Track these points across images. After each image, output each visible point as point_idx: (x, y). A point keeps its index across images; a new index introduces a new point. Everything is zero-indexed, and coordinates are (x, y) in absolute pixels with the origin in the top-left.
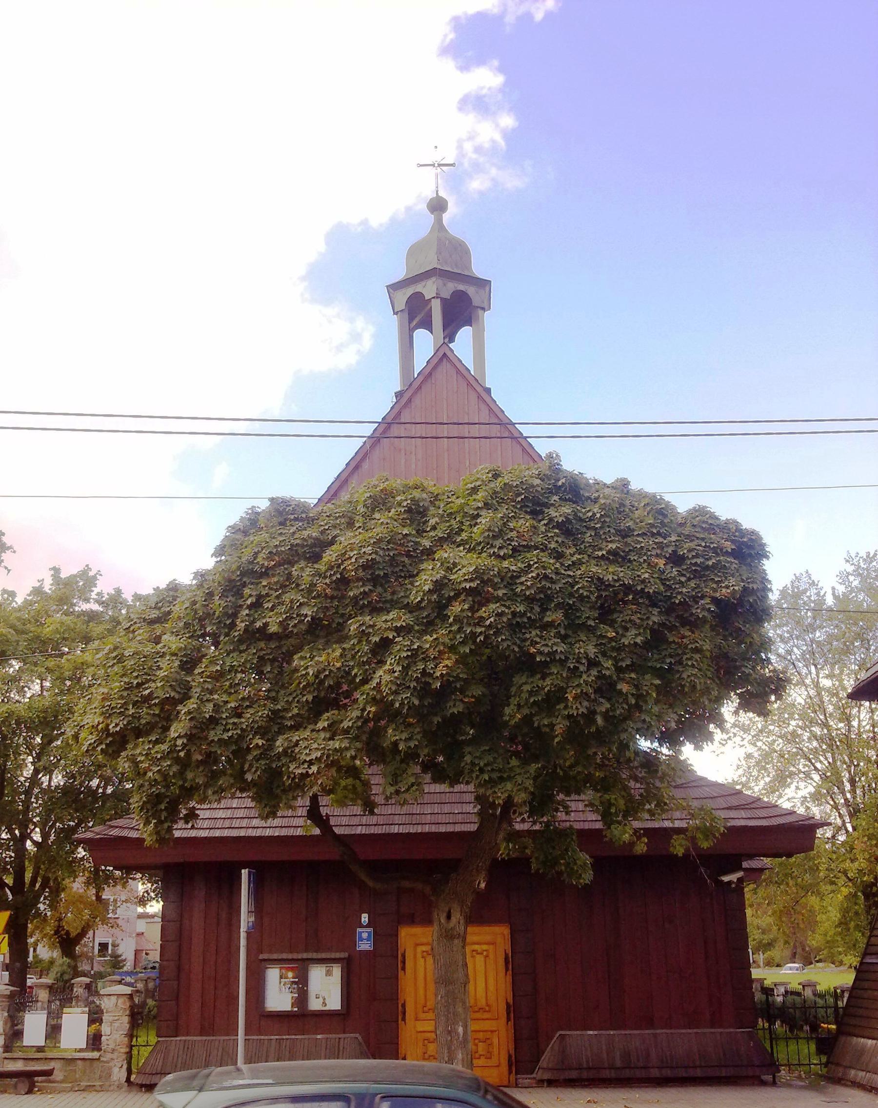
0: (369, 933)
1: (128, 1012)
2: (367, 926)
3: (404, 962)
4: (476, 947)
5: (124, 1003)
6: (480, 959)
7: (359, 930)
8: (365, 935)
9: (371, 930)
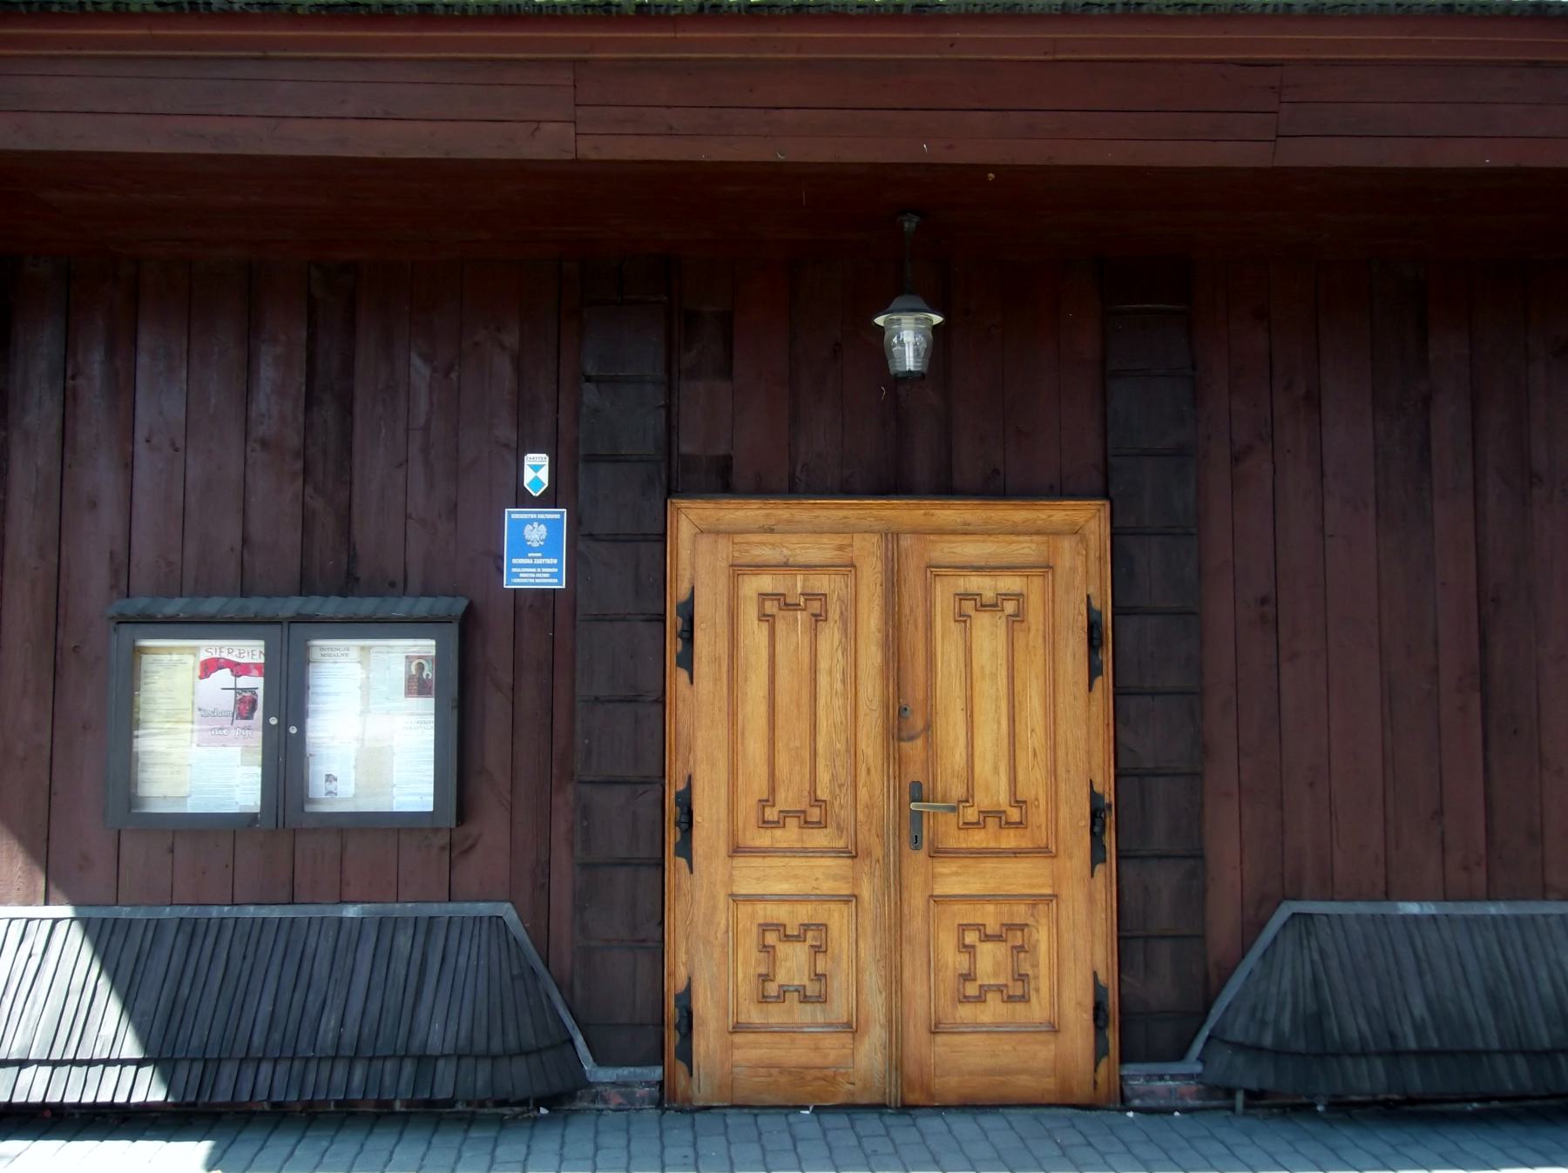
2: (550, 499)
3: (688, 635)
4: (975, 583)
6: (988, 634)
7: (513, 514)
9: (559, 514)
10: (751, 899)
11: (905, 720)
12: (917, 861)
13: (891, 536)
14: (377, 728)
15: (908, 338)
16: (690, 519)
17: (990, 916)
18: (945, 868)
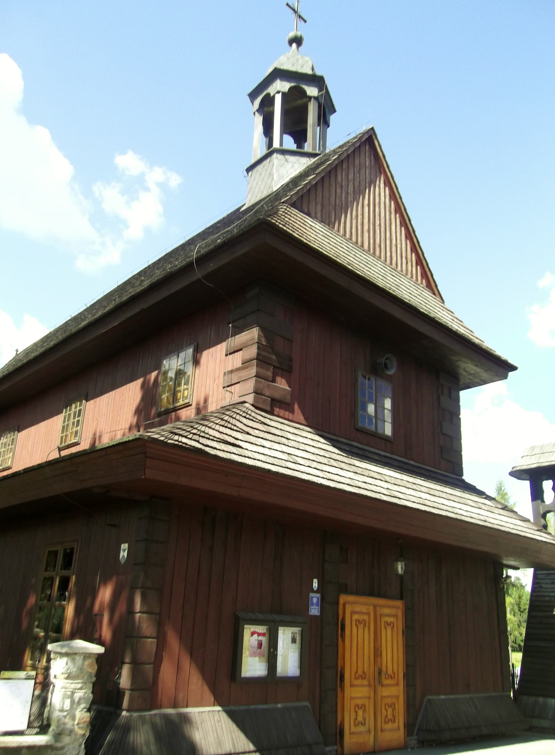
0: (318, 598)
1: (94, 679)
2: (317, 592)
5: (91, 665)
6: (389, 629)
7: (312, 595)
8: (315, 600)
9: (318, 595)
10: (354, 698)
11: (377, 652)
12: (379, 688)
13: (375, 607)
14: (289, 661)
15: (400, 568)
16: (343, 598)
17: (389, 701)
18: (384, 689)
